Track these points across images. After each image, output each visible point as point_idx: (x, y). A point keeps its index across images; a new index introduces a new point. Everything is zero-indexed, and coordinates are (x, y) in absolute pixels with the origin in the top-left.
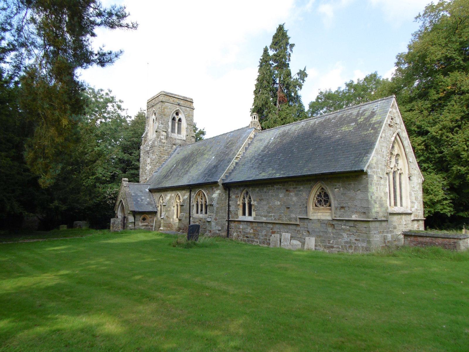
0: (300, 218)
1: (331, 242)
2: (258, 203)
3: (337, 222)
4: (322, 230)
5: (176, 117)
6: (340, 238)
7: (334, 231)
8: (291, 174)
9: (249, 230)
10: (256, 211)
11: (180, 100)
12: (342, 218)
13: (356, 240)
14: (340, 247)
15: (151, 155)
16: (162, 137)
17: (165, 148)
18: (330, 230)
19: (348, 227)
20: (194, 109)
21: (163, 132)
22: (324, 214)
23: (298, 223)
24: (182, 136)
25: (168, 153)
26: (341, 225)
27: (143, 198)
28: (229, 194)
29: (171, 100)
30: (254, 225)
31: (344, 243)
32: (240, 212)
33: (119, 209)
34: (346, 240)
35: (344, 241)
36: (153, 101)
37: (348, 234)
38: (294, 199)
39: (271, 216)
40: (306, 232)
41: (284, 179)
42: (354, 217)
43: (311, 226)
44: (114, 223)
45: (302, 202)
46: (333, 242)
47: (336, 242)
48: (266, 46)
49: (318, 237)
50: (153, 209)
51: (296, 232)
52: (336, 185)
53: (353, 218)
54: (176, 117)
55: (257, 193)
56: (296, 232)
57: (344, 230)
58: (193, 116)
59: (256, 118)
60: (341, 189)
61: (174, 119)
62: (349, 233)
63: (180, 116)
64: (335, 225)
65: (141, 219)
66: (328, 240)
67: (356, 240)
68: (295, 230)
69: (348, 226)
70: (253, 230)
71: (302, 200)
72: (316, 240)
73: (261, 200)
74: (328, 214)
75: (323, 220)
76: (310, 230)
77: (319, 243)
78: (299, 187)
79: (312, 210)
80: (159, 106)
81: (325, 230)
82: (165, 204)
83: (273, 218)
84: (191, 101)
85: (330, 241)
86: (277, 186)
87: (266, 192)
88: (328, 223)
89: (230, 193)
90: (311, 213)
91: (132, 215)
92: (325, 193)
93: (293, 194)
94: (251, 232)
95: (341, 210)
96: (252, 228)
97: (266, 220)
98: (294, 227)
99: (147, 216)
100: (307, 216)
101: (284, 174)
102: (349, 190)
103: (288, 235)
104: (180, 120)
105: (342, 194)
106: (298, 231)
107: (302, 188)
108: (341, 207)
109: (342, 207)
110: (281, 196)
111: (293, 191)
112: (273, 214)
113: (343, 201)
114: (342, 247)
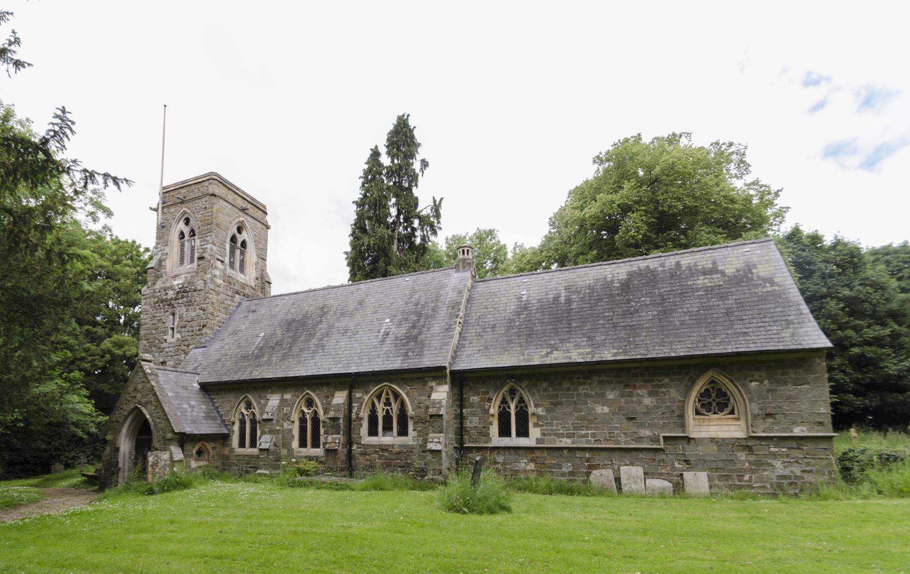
0: (665, 438)
1: (747, 478)
2: (548, 410)
3: (758, 442)
4: (724, 457)
5: (238, 235)
6: (766, 470)
7: (752, 458)
8: (715, 348)
9: (523, 465)
10: (541, 426)
11: (246, 202)
12: (787, 432)
13: (803, 471)
14: (768, 486)
15: (181, 310)
16: (217, 273)
17: (220, 297)
18: (742, 456)
19: (784, 450)
20: (268, 228)
21: (217, 261)
22: (723, 427)
23: (662, 446)
24: (247, 278)
25: (226, 309)
26: (767, 447)
27: (193, 403)
28: (461, 394)
29: (231, 197)
30: (538, 454)
31: (777, 479)
32: (494, 429)
33: (124, 430)
34: (780, 472)
35: (776, 474)
36: (183, 191)
37: (785, 462)
38: (648, 401)
39: (586, 436)
40: (681, 462)
41: (603, 364)
42: (797, 431)
43: (691, 451)
44: (155, 464)
45: (667, 407)
46: (750, 477)
47: (757, 477)
48: (376, 147)
49: (714, 470)
50: (218, 429)
51: (657, 463)
52: (753, 376)
53: (795, 433)
54: (238, 235)
55: (545, 390)
56: (657, 463)
57: (775, 456)
58: (266, 241)
59: (466, 252)
60: (766, 382)
61: (233, 239)
62: (787, 460)
63: (244, 236)
64: (754, 448)
65: (194, 452)
66: (738, 476)
67: (803, 471)
68: (654, 460)
69: (783, 448)
70: (536, 464)
71: (668, 404)
72: (708, 476)
73: (555, 405)
74: (733, 428)
75: (723, 439)
76: (692, 459)
77: (717, 482)
78: (659, 378)
79: (692, 420)
80: (201, 203)
81: (731, 458)
82: (270, 417)
83: (593, 440)
84: (264, 209)
85: (743, 476)
86: (600, 376)
87: (568, 389)
88: (737, 444)
89: (464, 391)
90: (691, 427)
91: (176, 444)
92: (719, 390)
93: (644, 391)
94: (528, 468)
95: (766, 420)
96: (532, 460)
97: (573, 443)
98: (651, 455)
99: (208, 445)
100: (683, 431)
101: (615, 355)
102: (785, 383)
103: (637, 471)
104: (244, 244)
105: (768, 391)
106: (660, 462)
107: (666, 381)
108: (766, 415)
109: (769, 415)
110: (611, 396)
111: (644, 387)
112: (590, 432)
113: (770, 403)
114: (772, 485)
